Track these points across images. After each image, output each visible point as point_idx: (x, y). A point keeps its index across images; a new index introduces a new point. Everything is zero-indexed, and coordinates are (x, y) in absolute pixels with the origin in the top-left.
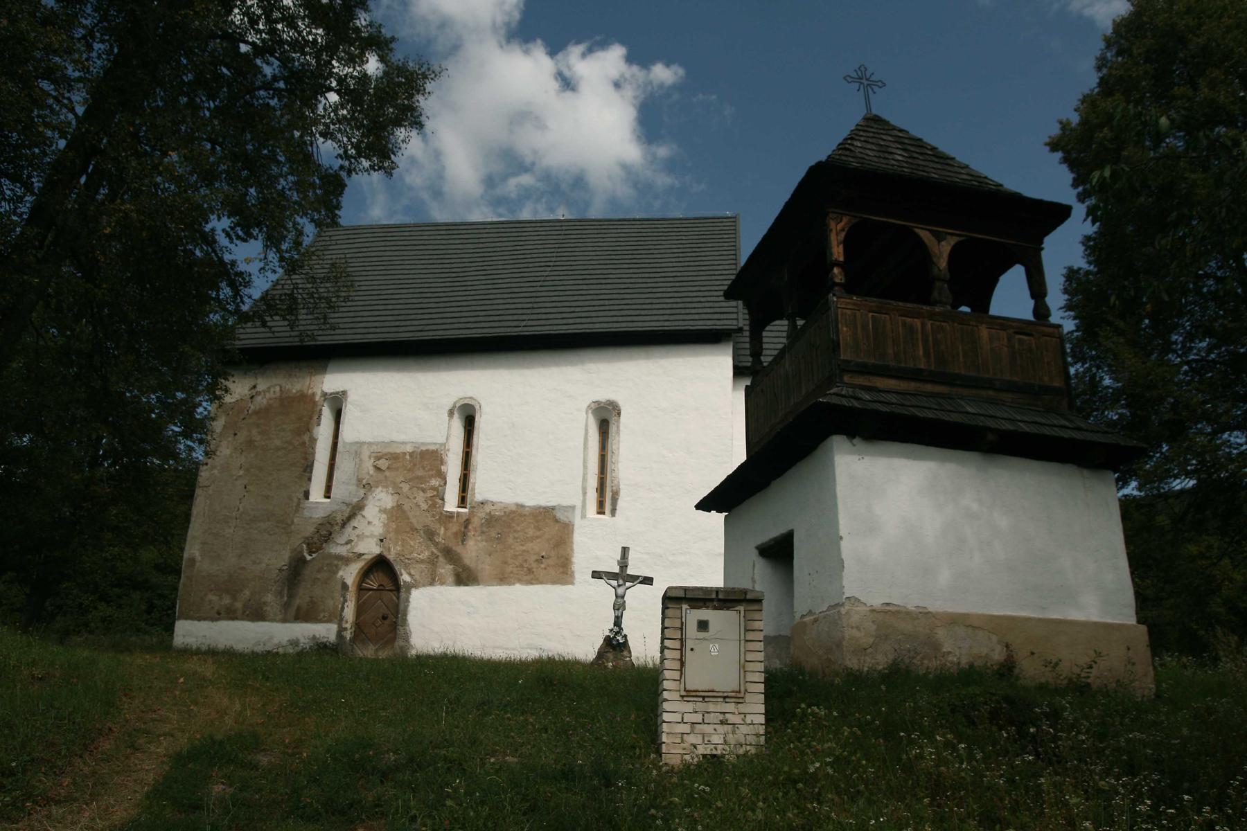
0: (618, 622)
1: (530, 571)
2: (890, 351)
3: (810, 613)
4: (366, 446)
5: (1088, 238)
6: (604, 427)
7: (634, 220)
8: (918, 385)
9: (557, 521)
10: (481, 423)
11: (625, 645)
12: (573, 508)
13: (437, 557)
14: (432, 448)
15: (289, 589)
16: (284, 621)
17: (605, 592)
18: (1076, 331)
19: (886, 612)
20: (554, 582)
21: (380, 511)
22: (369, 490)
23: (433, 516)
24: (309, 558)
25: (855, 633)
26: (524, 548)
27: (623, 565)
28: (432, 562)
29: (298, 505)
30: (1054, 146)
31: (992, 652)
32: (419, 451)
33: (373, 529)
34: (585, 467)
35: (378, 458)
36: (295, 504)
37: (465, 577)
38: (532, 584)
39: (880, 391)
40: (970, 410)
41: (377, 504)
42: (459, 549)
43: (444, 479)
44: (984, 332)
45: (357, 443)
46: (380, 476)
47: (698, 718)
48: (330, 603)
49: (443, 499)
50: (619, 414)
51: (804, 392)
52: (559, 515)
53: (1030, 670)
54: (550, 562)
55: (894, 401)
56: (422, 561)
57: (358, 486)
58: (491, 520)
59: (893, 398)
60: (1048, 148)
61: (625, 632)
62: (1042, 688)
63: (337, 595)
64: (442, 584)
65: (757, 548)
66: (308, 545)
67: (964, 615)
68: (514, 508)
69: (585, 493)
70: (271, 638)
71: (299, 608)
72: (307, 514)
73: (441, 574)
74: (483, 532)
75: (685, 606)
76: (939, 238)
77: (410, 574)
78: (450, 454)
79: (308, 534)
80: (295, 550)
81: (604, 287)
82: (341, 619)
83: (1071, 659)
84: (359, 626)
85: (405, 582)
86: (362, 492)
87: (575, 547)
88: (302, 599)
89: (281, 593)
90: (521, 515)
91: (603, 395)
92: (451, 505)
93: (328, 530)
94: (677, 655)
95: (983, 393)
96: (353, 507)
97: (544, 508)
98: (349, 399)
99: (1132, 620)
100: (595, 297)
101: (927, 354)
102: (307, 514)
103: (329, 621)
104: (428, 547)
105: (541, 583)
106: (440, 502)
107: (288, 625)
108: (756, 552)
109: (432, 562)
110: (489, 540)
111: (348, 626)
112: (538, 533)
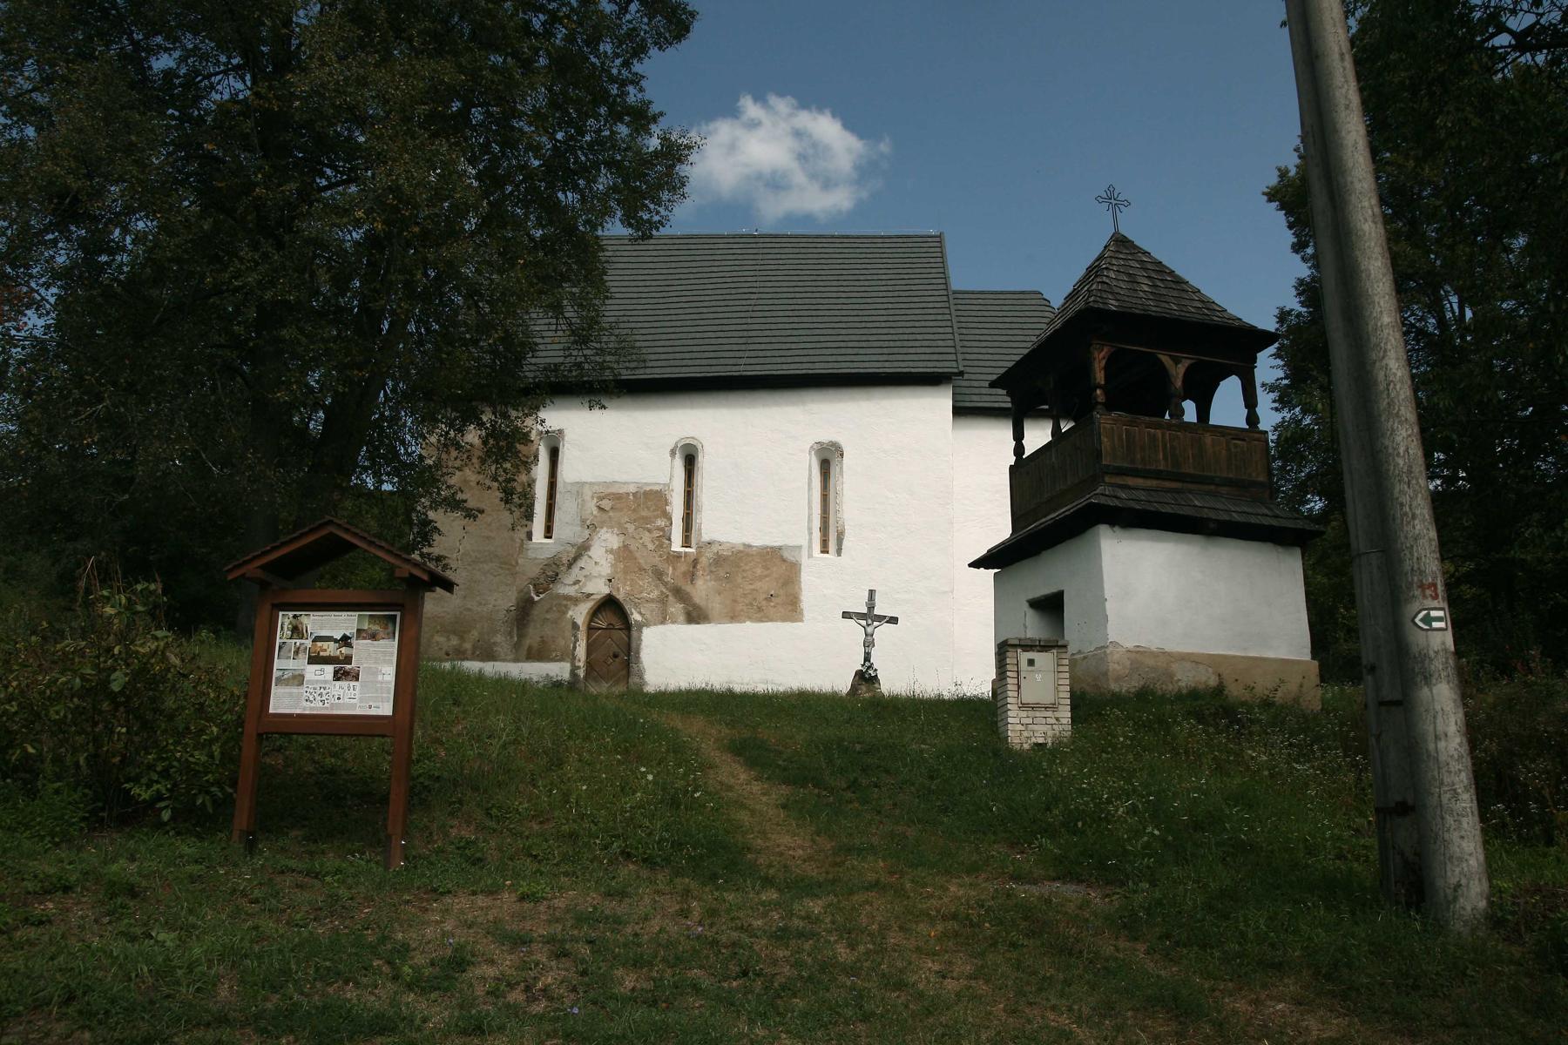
0: (867, 658)
1: (760, 609)
2: (1139, 456)
3: (1080, 652)
4: (588, 486)
5: (1301, 282)
7: (833, 237)
8: (1159, 482)
9: (784, 561)
10: (704, 463)
11: (874, 680)
12: (800, 547)
13: (667, 596)
14: (657, 488)
15: (518, 629)
16: (516, 660)
17: (855, 630)
18: (1286, 378)
19: (1137, 652)
20: (784, 619)
21: (606, 551)
22: (594, 531)
23: (661, 556)
24: (536, 598)
25: (1116, 666)
26: (752, 587)
27: (871, 607)
28: (662, 601)
30: (1272, 195)
31: (1208, 679)
32: (642, 491)
33: (600, 569)
34: (810, 508)
35: (601, 499)
36: (518, 545)
37: (695, 616)
38: (762, 621)
39: (1134, 489)
40: (1198, 504)
41: (603, 544)
42: (688, 588)
43: (670, 519)
44: (1208, 439)
45: (578, 483)
46: (605, 516)
49: (670, 539)
50: (842, 455)
51: (1069, 483)
52: (786, 555)
53: (1235, 691)
54: (778, 600)
55: (1143, 498)
56: (652, 601)
57: (582, 526)
58: (719, 560)
59: (1142, 495)
60: (1265, 198)
61: (875, 667)
62: (1243, 704)
63: (568, 633)
64: (673, 622)
65: (1028, 601)
66: (535, 586)
67: (1188, 654)
68: (741, 548)
69: (810, 534)
71: (530, 648)
72: (531, 554)
73: (672, 613)
74: (711, 572)
75: (1019, 650)
76: (1177, 361)
77: (640, 613)
78: (674, 494)
79: (533, 575)
80: (522, 591)
81: (815, 319)
82: (573, 658)
83: (1263, 685)
84: (590, 665)
85: (635, 621)
86: (587, 532)
88: (533, 637)
89: (510, 634)
90: (748, 555)
91: (826, 437)
92: (677, 546)
93: (552, 572)
94: (1015, 681)
95: (1206, 487)
96: (579, 548)
97: (772, 548)
98: (566, 438)
99: (1305, 654)
100: (808, 332)
101: (1165, 458)
102: (531, 554)
103: (561, 660)
104: (656, 586)
105: (771, 620)
107: (520, 664)
108: (1027, 604)
109: (662, 601)
110: (718, 579)
111: (581, 664)
112: (766, 573)
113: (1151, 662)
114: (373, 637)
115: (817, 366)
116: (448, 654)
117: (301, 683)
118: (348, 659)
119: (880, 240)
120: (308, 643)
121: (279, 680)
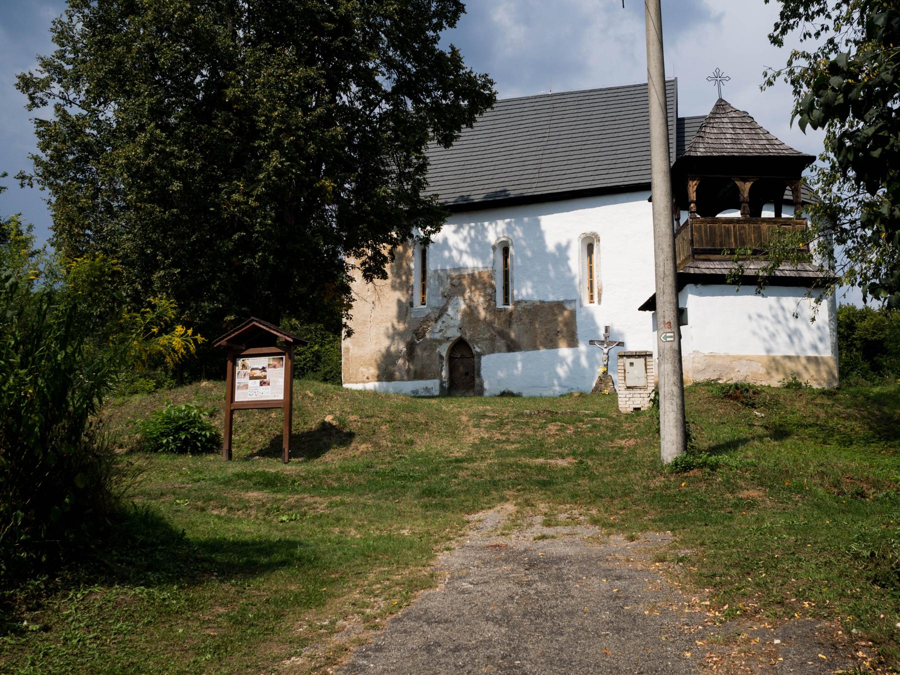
6: (590, 249)
28: (492, 340)
29: (407, 310)
37: (512, 347)
42: (507, 330)
47: (631, 396)
48: (434, 367)
49: (495, 301)
50: (599, 240)
56: (486, 339)
64: (499, 352)
70: (401, 390)
86: (445, 300)
87: (578, 324)
90: (543, 308)
91: (589, 229)
92: (500, 305)
101: (736, 241)
103: (435, 378)
104: (489, 331)
106: (493, 303)
113: (719, 362)
114: (275, 367)
115: (581, 184)
116: (368, 378)
117: (247, 388)
118: (265, 377)
119: (633, 89)
120: (249, 371)
121: (238, 387)
